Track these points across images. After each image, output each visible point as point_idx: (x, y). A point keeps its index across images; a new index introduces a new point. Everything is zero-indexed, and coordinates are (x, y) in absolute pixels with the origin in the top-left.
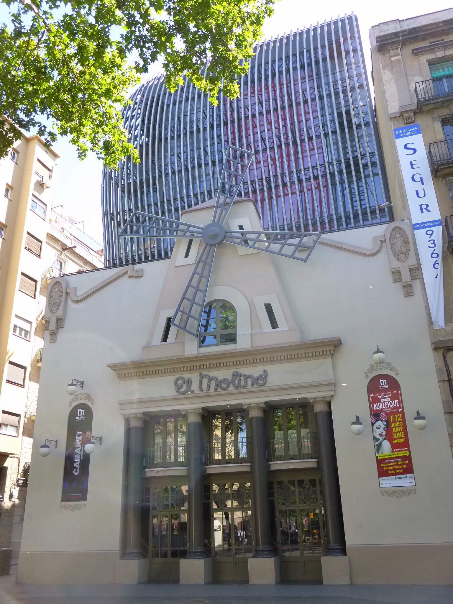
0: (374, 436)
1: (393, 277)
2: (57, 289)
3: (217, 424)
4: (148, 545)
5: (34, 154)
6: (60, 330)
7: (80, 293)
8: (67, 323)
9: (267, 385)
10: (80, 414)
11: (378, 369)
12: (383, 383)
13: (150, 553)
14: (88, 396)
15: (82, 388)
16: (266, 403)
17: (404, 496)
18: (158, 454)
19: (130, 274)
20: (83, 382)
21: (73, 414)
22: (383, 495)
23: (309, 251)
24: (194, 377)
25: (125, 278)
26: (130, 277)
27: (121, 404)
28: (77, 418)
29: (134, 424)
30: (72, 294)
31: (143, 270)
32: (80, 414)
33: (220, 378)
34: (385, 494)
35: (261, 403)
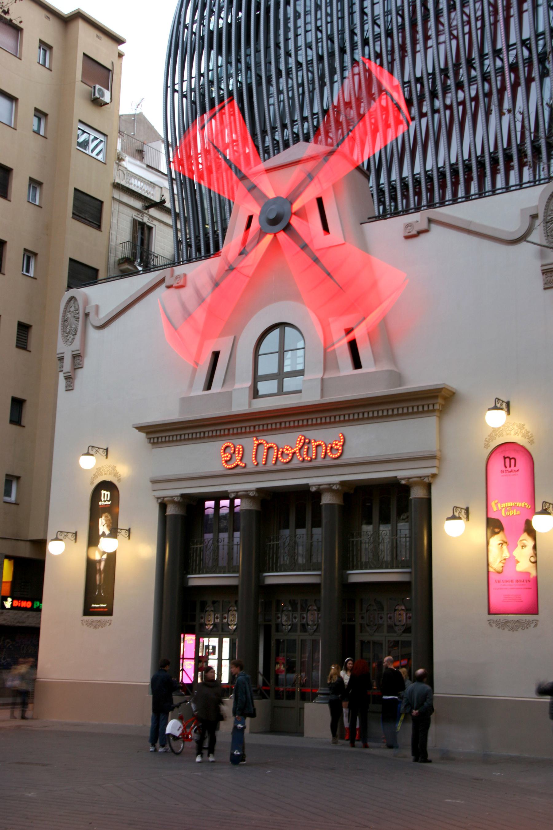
0: (535, 539)
1: (544, 280)
2: (72, 309)
5: (76, 46)
6: (79, 372)
7: (104, 314)
8: (88, 362)
9: (344, 457)
16: (183, 496)
17: (520, 629)
18: (208, 556)
19: (168, 282)
22: (491, 625)
25: (161, 290)
26: (169, 287)
27: (154, 482)
29: (171, 510)
30: (92, 316)
31: (185, 275)
34: (494, 625)
35: (334, 484)
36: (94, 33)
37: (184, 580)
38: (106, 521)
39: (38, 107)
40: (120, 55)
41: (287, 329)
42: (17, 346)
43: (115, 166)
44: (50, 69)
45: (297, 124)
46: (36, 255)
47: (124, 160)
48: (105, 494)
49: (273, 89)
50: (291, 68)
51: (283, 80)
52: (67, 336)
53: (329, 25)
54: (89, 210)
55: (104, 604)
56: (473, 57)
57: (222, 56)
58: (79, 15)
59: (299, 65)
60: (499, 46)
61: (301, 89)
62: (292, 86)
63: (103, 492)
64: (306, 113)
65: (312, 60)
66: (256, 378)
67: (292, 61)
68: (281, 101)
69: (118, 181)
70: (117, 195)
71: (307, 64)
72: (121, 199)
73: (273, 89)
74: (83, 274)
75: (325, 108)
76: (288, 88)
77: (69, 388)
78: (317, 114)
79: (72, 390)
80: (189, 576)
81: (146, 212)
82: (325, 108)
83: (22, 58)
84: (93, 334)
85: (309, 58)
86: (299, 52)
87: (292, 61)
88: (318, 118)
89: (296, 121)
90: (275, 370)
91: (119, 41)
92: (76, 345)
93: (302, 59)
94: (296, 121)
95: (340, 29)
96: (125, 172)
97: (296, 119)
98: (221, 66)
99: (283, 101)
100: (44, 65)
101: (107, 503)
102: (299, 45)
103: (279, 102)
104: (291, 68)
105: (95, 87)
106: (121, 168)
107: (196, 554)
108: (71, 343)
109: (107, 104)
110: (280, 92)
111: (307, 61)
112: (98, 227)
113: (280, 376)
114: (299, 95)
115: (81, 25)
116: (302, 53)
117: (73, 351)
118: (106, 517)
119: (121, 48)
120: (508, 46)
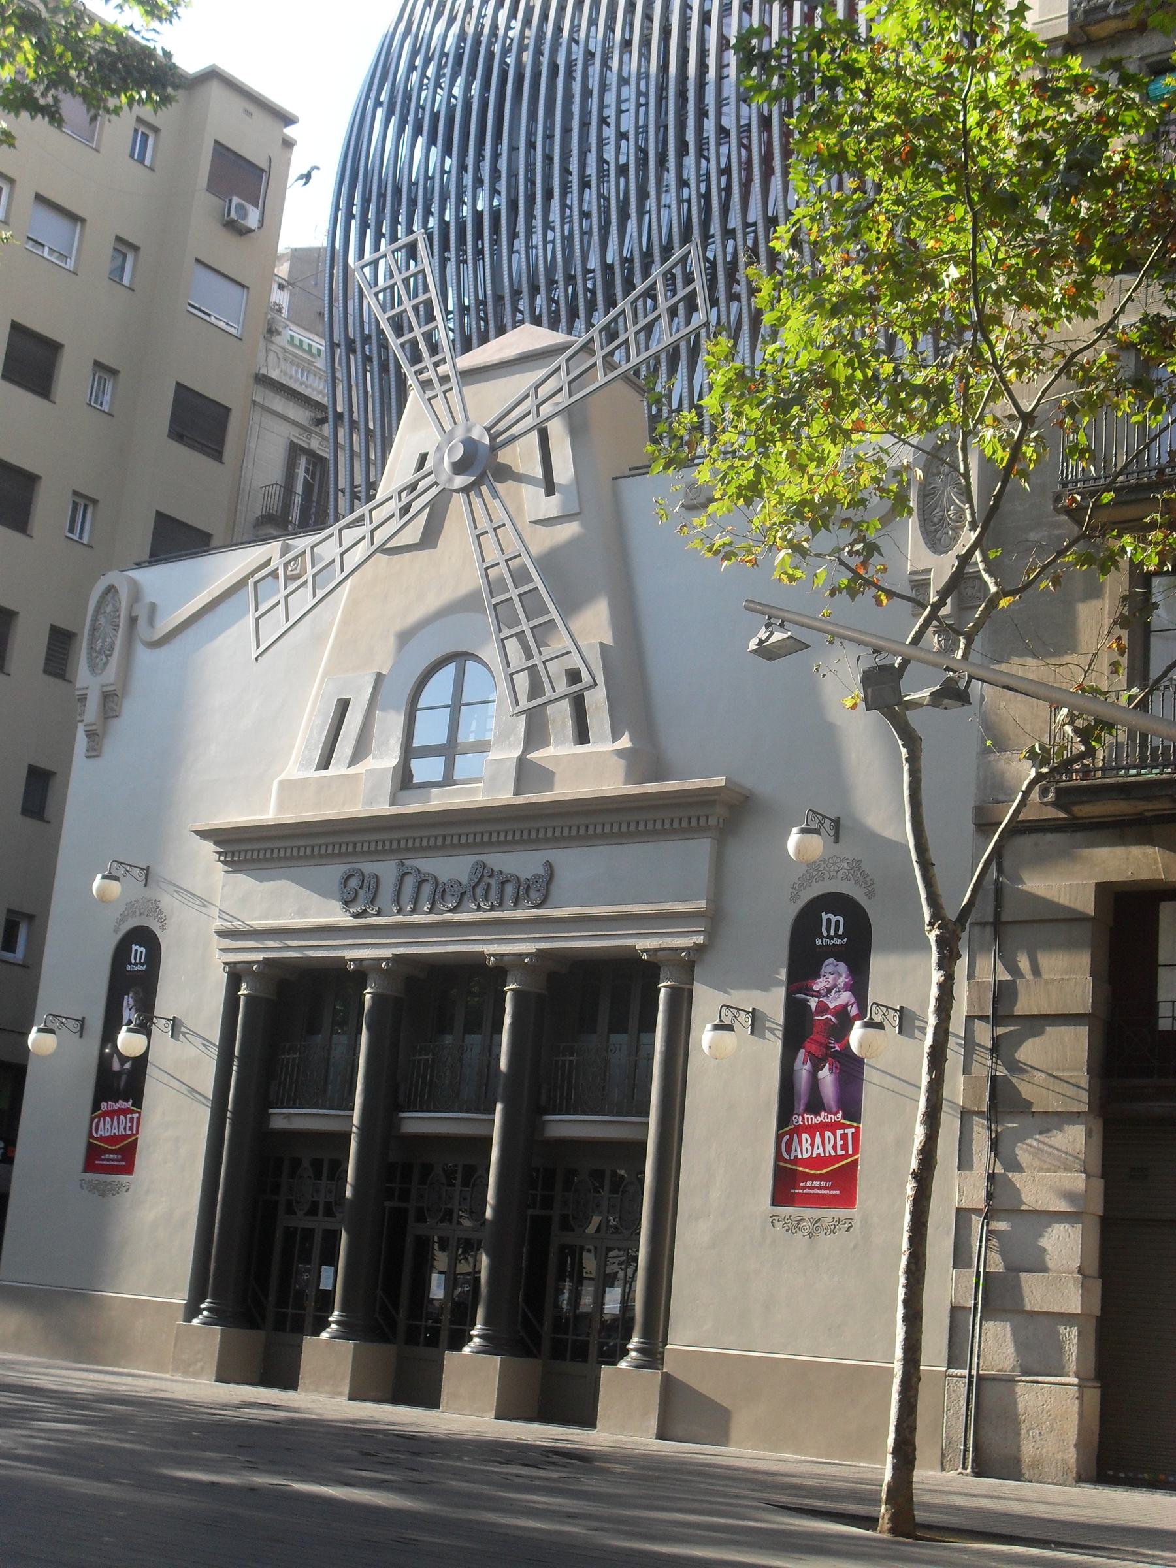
3: (835, 1001)
4: (542, 1325)
8: (131, 709)
10: (828, 929)
11: (827, 876)
12: (833, 922)
13: (546, 1344)
14: (155, 910)
15: (837, 841)
20: (837, 822)
21: (121, 953)
23: (388, 546)
24: (386, 870)
28: (128, 968)
30: (142, 622)
32: (828, 929)
33: (525, 874)
34: (779, 1225)
36: (239, 104)
37: (264, 1118)
38: (135, 1001)
39: (121, 235)
40: (288, 144)
41: (470, 664)
42: (46, 671)
43: (262, 344)
44: (151, 169)
45: (713, 243)
46: (95, 502)
47: (279, 333)
48: (138, 951)
49: (671, 177)
50: (707, 138)
51: (690, 160)
52: (936, 531)
53: (642, 109)
54: (199, 423)
55: (497, 1209)
56: (712, 232)
57: (450, 157)
58: (213, 75)
59: (723, 132)
60: (731, 226)
61: (724, 179)
62: (708, 173)
63: (134, 947)
64: (734, 222)
65: (749, 125)
66: (409, 752)
67: (710, 125)
68: (683, 201)
69: (263, 371)
70: (263, 396)
71: (739, 132)
72: (267, 404)
73: (671, 177)
74: (177, 539)
75: (770, 214)
76: (698, 175)
77: (94, 752)
78: (755, 224)
79: (97, 756)
80: (272, 1111)
81: (317, 430)
82: (770, 214)
83: (101, 150)
84: (144, 656)
85: (743, 122)
86: (724, 109)
87: (710, 125)
88: (755, 232)
89: (713, 236)
90: (442, 739)
91: (288, 120)
92: (110, 674)
93: (729, 122)
94: (713, 236)
95: (641, 123)
96: (281, 356)
97: (712, 232)
98: (449, 172)
99: (689, 201)
100: (141, 160)
101: (139, 968)
102: (725, 95)
103: (680, 201)
104: (707, 138)
105: (230, 201)
106: (274, 348)
107: (562, 1094)
108: (103, 669)
109: (250, 231)
110: (683, 183)
111: (739, 126)
112: (217, 454)
113: (449, 750)
114: (720, 190)
115: (215, 88)
116: (729, 110)
117: (103, 686)
118: (135, 993)
119: (290, 131)
120: (746, 225)
